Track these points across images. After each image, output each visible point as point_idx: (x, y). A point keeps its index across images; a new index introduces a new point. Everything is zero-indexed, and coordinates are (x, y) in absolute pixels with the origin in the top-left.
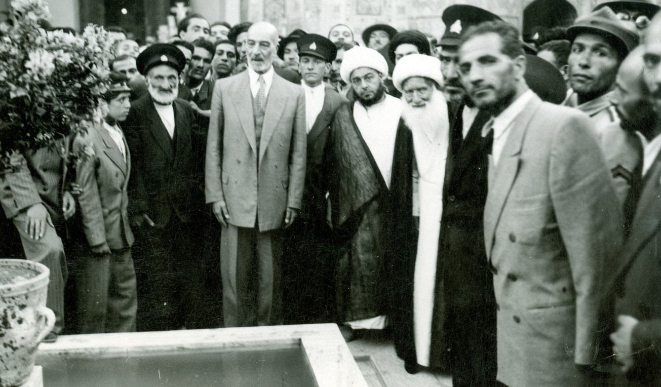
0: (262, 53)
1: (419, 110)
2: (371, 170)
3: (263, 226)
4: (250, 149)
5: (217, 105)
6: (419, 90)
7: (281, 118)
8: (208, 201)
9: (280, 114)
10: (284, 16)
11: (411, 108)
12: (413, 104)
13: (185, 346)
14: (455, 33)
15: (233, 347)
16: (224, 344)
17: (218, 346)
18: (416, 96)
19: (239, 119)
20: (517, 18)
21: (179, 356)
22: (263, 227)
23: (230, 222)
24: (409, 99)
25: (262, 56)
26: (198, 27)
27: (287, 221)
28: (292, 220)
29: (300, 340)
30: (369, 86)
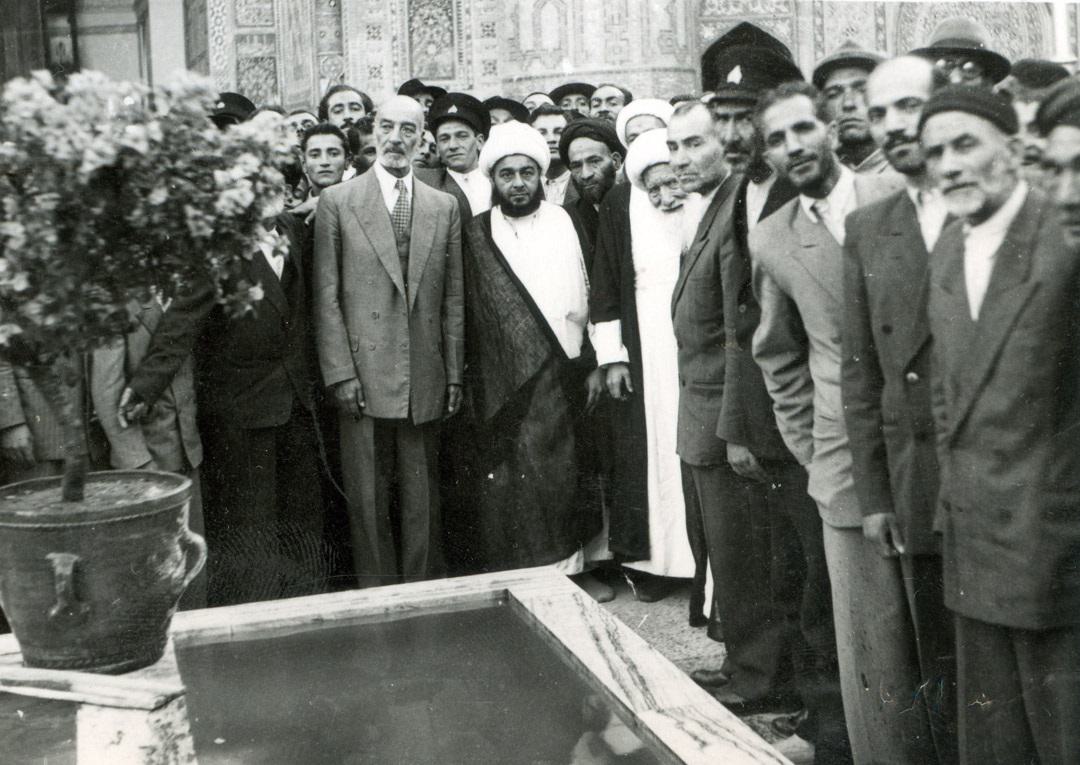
0: (404, 143)
1: (674, 216)
2: (532, 322)
3: (418, 417)
4: (395, 289)
5: (334, 229)
6: (668, 183)
7: (433, 244)
8: (329, 382)
9: (431, 238)
10: (275, 90)
11: (663, 214)
12: (662, 207)
13: (325, 617)
14: (732, 84)
15: (401, 613)
16: (387, 609)
17: (375, 612)
18: (666, 194)
19: (370, 243)
20: (692, 71)
21: (315, 633)
22: (419, 418)
23: (367, 412)
24: (656, 200)
25: (402, 146)
26: (340, 105)
27: (451, 409)
28: (458, 406)
29: (506, 592)
30: (525, 185)
